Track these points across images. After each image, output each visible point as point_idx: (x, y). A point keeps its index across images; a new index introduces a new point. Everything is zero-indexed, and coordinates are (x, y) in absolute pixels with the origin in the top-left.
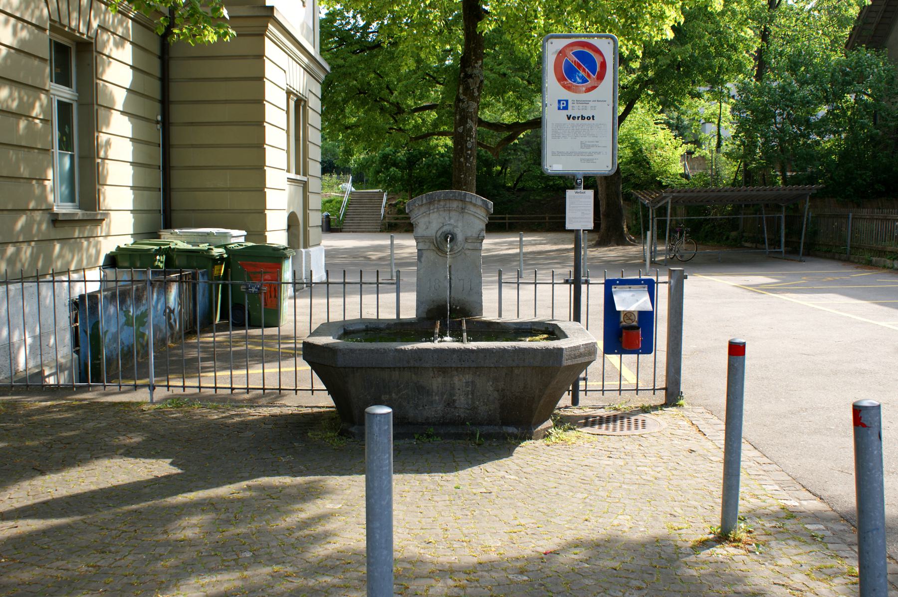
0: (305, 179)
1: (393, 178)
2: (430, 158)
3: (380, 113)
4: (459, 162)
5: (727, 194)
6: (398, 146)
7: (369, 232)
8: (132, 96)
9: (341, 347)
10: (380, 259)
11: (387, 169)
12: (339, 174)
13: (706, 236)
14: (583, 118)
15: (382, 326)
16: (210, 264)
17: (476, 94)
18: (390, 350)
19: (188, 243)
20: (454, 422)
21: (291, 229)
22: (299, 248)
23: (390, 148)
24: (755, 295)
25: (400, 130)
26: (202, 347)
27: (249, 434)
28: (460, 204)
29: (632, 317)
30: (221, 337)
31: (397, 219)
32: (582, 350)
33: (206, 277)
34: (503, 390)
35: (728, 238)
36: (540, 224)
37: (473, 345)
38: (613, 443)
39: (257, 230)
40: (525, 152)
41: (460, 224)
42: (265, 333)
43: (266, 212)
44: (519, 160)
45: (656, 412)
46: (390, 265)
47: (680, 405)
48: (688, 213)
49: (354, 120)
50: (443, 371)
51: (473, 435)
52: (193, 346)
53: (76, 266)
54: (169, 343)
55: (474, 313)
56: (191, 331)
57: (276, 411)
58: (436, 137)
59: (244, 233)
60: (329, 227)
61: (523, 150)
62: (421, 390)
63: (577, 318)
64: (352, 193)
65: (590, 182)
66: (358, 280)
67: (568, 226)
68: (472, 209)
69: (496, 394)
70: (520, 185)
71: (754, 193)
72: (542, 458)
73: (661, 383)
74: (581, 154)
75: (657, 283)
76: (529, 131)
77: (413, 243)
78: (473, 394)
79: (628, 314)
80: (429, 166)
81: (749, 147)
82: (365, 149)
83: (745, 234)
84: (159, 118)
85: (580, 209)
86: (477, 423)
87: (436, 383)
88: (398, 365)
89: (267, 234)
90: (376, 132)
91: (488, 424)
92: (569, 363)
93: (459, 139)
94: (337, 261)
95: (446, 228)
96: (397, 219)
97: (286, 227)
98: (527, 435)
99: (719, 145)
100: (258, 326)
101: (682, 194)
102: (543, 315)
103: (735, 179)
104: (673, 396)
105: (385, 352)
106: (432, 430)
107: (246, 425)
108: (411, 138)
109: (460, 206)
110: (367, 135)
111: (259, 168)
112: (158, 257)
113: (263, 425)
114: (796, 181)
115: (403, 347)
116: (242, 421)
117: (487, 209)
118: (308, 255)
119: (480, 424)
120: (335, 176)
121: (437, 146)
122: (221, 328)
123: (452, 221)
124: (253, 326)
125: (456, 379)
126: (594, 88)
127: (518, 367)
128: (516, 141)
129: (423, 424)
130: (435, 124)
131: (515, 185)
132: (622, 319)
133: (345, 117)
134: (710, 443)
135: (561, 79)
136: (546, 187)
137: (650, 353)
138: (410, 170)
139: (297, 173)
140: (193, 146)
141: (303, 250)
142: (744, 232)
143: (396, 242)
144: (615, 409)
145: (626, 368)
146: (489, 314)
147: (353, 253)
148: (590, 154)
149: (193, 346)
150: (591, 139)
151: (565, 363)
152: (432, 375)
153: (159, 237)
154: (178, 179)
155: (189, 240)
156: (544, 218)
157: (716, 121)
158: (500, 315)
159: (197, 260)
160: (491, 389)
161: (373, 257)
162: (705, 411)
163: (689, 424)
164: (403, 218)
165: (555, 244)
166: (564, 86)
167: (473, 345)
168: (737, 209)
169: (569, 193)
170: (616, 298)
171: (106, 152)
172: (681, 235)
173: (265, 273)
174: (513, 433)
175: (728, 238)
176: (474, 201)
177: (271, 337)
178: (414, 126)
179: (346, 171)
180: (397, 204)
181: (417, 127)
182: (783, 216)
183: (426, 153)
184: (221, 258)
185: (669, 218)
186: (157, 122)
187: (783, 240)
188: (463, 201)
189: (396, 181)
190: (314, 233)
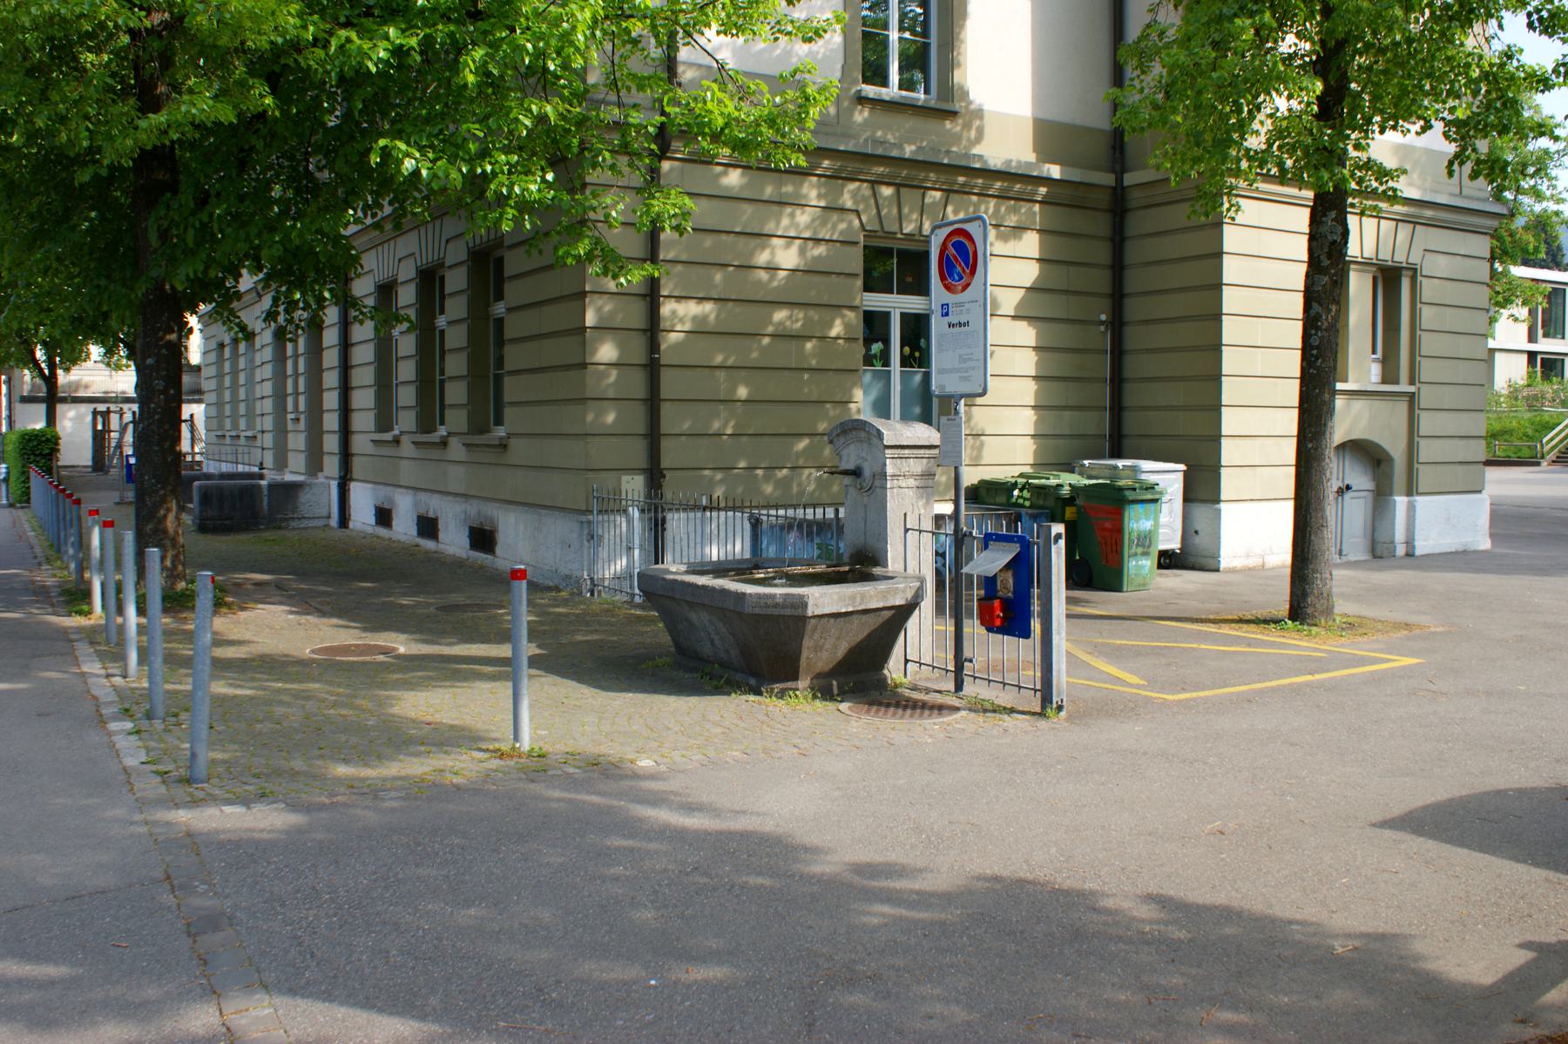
14: (960, 324)
135: (943, 278)
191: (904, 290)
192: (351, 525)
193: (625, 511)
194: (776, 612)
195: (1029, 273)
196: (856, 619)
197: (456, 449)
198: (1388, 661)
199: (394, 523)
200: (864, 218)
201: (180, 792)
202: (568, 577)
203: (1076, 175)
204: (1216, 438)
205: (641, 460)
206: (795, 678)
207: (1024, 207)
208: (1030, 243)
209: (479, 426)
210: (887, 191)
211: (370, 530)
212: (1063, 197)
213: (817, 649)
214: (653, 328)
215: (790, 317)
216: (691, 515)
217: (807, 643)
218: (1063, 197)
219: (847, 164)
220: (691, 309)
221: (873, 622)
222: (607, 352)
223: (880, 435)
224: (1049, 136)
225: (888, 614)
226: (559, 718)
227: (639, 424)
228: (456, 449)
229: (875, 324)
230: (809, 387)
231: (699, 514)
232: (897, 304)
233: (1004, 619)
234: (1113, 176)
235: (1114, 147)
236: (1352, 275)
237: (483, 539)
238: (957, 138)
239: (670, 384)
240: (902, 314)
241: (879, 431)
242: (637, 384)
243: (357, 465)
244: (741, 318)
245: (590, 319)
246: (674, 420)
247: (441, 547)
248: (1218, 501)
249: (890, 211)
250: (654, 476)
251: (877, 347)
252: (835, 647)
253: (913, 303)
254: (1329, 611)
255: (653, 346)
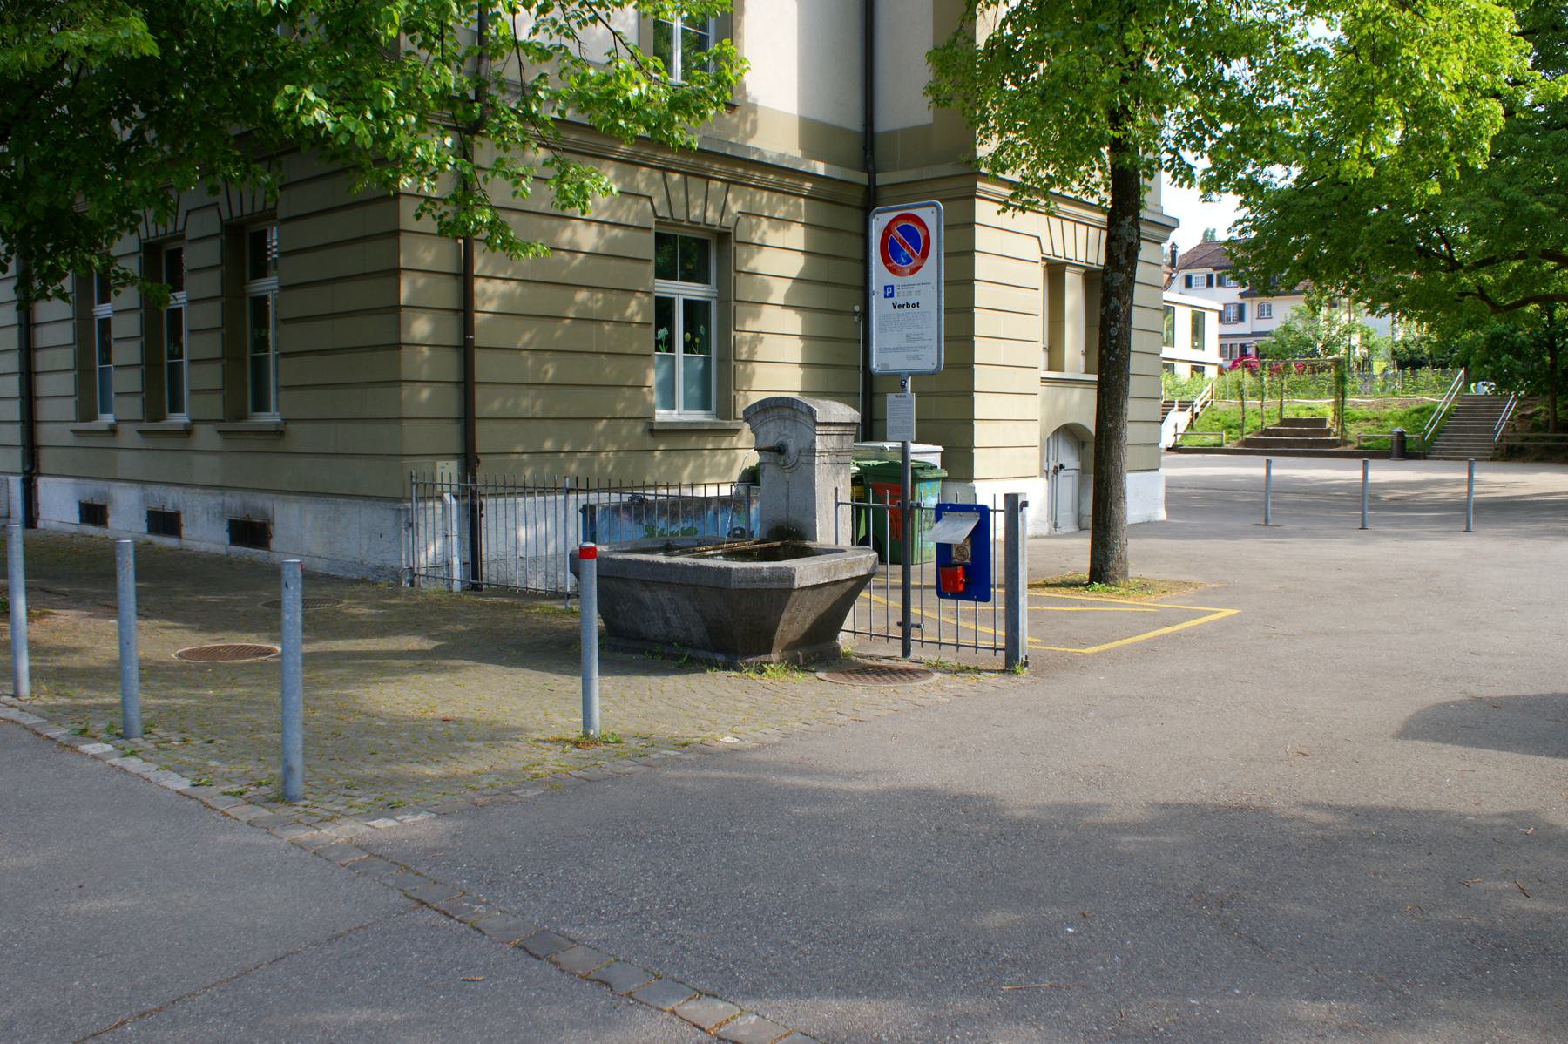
8: (803, 285)
14: (908, 306)
17: (1124, 262)
42: (1002, 581)
53: (691, 476)
84: (857, 308)
96: (1527, 439)
126: (918, 268)
135: (886, 260)
166: (890, 269)
171: (752, 351)
180: (1533, 415)
191: (688, 277)
192: (40, 524)
193: (440, 498)
194: (763, 586)
195: (795, 264)
196: (826, 591)
197: (206, 436)
198: (1204, 614)
199: (110, 520)
200: (656, 202)
201: (283, 811)
202: (377, 569)
203: (837, 173)
204: (968, 421)
205: (454, 442)
206: (768, 651)
207: (792, 200)
208: (796, 236)
209: (153, 411)
210: (676, 177)
211: (73, 529)
212: (826, 194)
213: (792, 620)
214: (465, 309)
215: (591, 298)
216: (550, 498)
217: (785, 616)
218: (826, 194)
219: (653, 147)
220: (497, 287)
221: (838, 592)
222: (421, 328)
223: (811, 412)
224: (815, 134)
225: (851, 584)
226: (536, 711)
227: (452, 407)
228: (206, 436)
229: (664, 309)
230: (610, 371)
231: (561, 497)
232: (682, 291)
233: (966, 585)
234: (866, 176)
235: (865, 148)
236: (1068, 275)
237: (250, 532)
238: (736, 130)
239: (484, 366)
240: (685, 301)
241: (810, 408)
242: (450, 366)
243: (46, 459)
244: (544, 300)
245: (405, 294)
246: (488, 403)
247: (186, 543)
248: (970, 479)
249: (678, 196)
250: (469, 461)
251: (663, 332)
252: (805, 619)
253: (696, 291)
254: (1125, 574)
255: (467, 326)
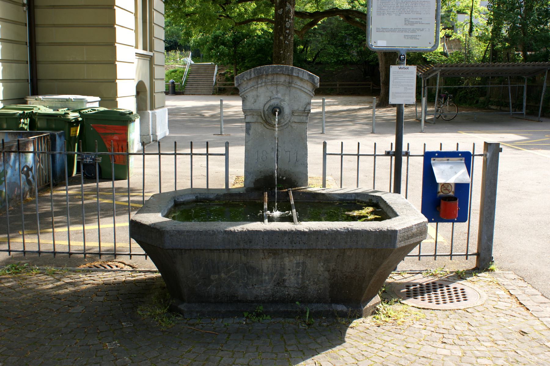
0: (151, 54)
1: (222, 54)
2: (250, 39)
3: (212, 3)
4: (279, 39)
5: (483, 68)
6: (226, 29)
7: (204, 94)
9: (168, 228)
10: (212, 116)
11: (217, 47)
12: (181, 51)
13: (460, 100)
15: (212, 197)
16: (67, 126)
18: (219, 232)
19: (50, 107)
20: (283, 301)
21: (140, 95)
22: (146, 110)
23: (220, 31)
24: (518, 152)
25: (228, 16)
26: (55, 201)
27: (79, 308)
28: (287, 79)
29: (450, 188)
30: (73, 190)
31: (225, 85)
32: (414, 231)
33: (63, 138)
34: (334, 270)
35: (477, 102)
36: (332, 89)
37: (305, 226)
38: (441, 320)
39: (109, 97)
40: (322, 35)
41: (287, 98)
43: (117, 81)
44: (317, 41)
45: (470, 279)
46: (220, 121)
47: (492, 270)
48: (446, 82)
49: (192, 9)
50: (274, 253)
51: (303, 313)
52: (49, 200)
54: (28, 197)
55: (299, 183)
56: (46, 186)
57: (109, 277)
58: (255, 22)
59: (98, 99)
60: (174, 90)
61: (320, 34)
62: (251, 270)
63: (397, 190)
64: (191, 65)
65: (415, 58)
66: (190, 152)
67: (392, 101)
68: (299, 83)
69: (326, 274)
70: (317, 60)
71: (505, 68)
72: (377, 346)
73: (474, 249)
74: (405, 30)
75: (474, 155)
76: (326, 18)
77: (239, 103)
78: (303, 274)
79: (445, 186)
80: (249, 45)
81: (496, 31)
82: (200, 32)
83: (491, 99)
85: (403, 82)
86: (305, 301)
87: (266, 264)
88: (228, 247)
89: (118, 99)
90: (210, 19)
91: (317, 302)
92: (403, 244)
93: (279, 22)
94: (178, 118)
95: (273, 102)
96: (225, 85)
97: (135, 93)
98: (357, 313)
99: (471, 30)
100: (109, 179)
101: (448, 68)
102: (365, 187)
103: (484, 57)
104: (484, 262)
105: (214, 234)
106: (261, 308)
107: (78, 297)
108: (236, 23)
109: (287, 80)
110: (202, 20)
111: (110, 44)
112: (22, 120)
113: (95, 298)
114: (534, 59)
115: (232, 229)
116: (75, 292)
117: (313, 84)
118: (154, 116)
119: (310, 302)
120: (178, 52)
121: (256, 29)
122: (74, 181)
123: (279, 95)
124: (103, 178)
125: (287, 261)
127: (350, 249)
128: (316, 27)
129: (252, 302)
130: (255, 12)
131: (314, 60)
132: (439, 190)
133: (185, 6)
134: (537, 322)
136: (337, 62)
137: (465, 221)
138: (235, 48)
139: (145, 48)
140: (55, 26)
141: (150, 112)
142: (490, 97)
143: (224, 102)
144: (433, 275)
145: (439, 234)
146: (314, 185)
147: (191, 111)
148: (414, 31)
149: (49, 200)
150: (415, 16)
151: (399, 244)
152: (262, 256)
153: (26, 103)
154: (43, 53)
155: (51, 105)
156: (336, 85)
157: (469, 12)
158: (324, 185)
159: (55, 122)
160: (322, 269)
161: (207, 115)
162: (516, 277)
163: (507, 295)
164: (229, 85)
165: (345, 105)
167: (305, 226)
168: (485, 80)
169: (394, 69)
170: (435, 169)
172: (445, 99)
173: (114, 134)
174: (342, 311)
175: (477, 102)
176: (301, 76)
177: (118, 190)
178: (239, 14)
179: (187, 48)
180: (225, 74)
181: (240, 15)
182: (525, 86)
183: (247, 36)
184: (77, 121)
185: (438, 87)
186: (24, 5)
187: (525, 104)
188: (290, 75)
189: (225, 56)
190: (158, 97)
